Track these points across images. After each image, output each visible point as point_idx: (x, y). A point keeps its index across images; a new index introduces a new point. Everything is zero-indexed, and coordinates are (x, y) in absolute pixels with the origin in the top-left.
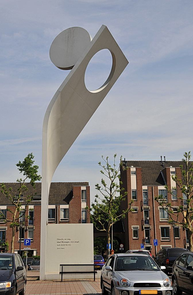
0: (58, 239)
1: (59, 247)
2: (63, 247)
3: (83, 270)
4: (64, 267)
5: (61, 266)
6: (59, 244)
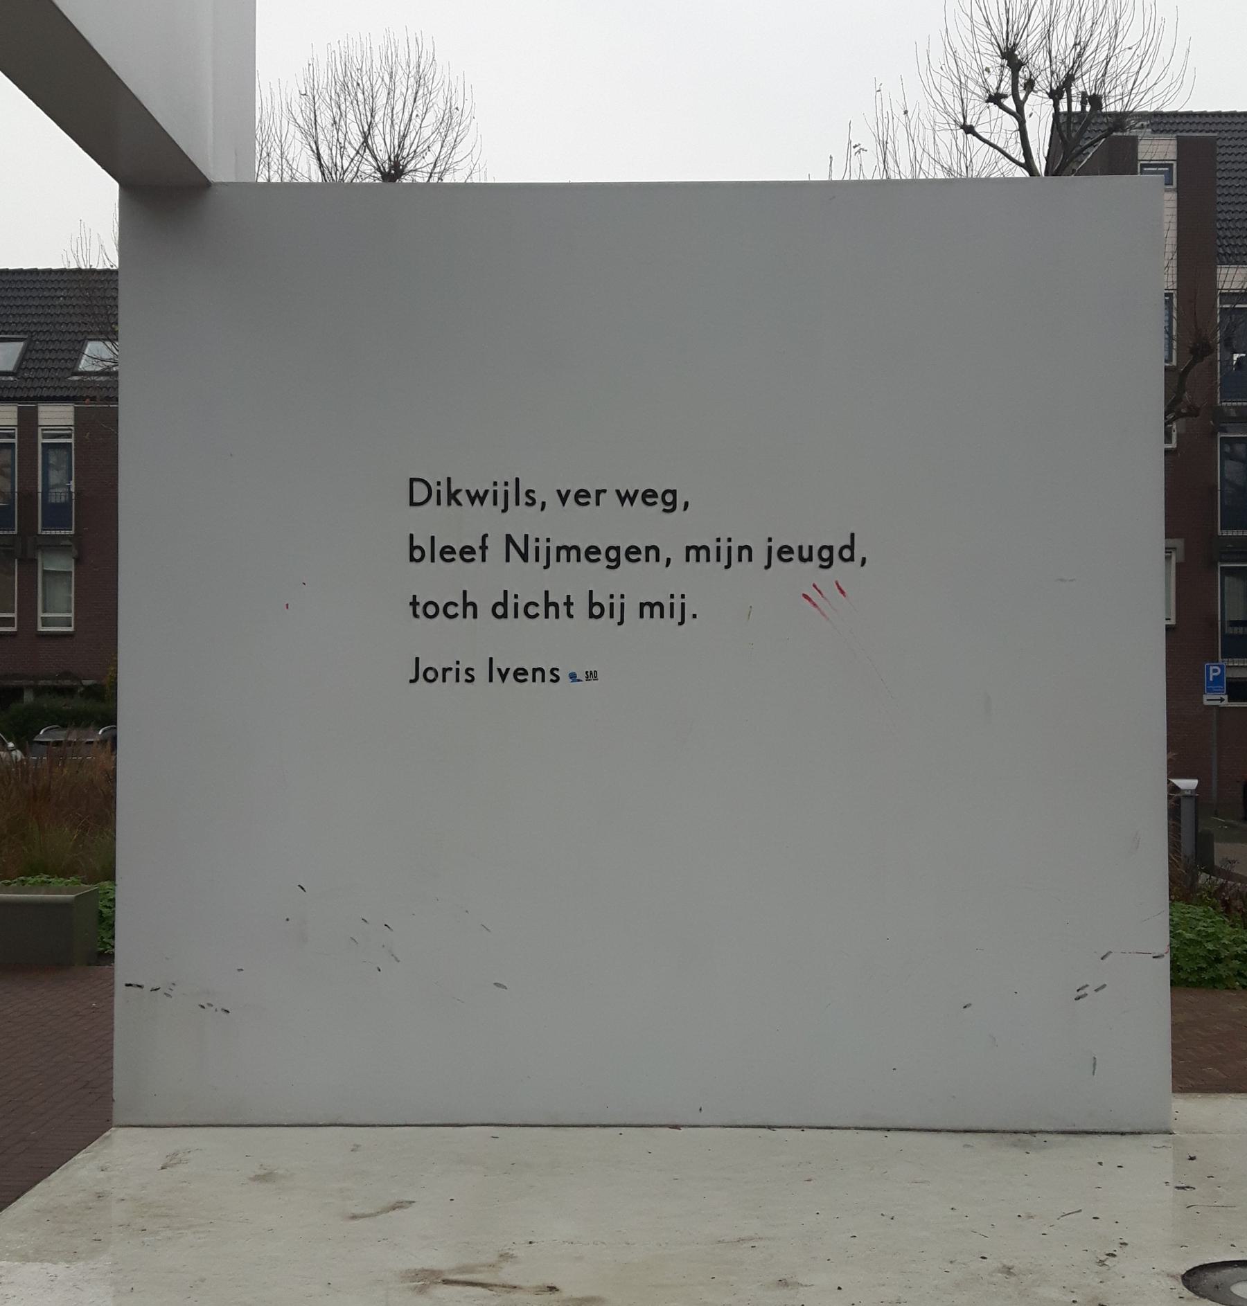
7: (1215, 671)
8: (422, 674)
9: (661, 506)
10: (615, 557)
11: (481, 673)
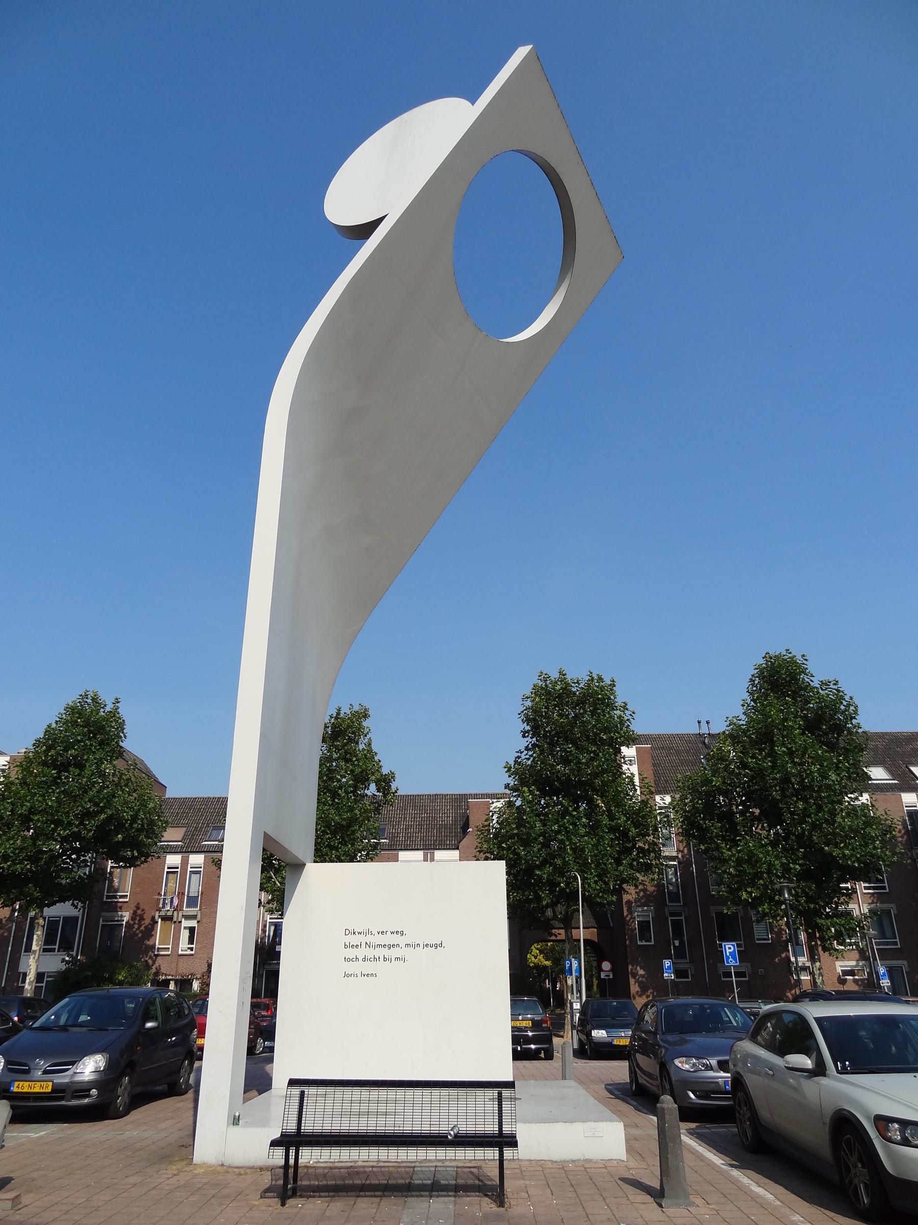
0: (348, 932)
1: (352, 968)
2: (369, 967)
3: (417, 1121)
4: (310, 1091)
5: (296, 1091)
6: (351, 953)
7: (730, 948)
8: (346, 975)
9: (387, 948)
10: (390, 947)
11: (359, 975)
